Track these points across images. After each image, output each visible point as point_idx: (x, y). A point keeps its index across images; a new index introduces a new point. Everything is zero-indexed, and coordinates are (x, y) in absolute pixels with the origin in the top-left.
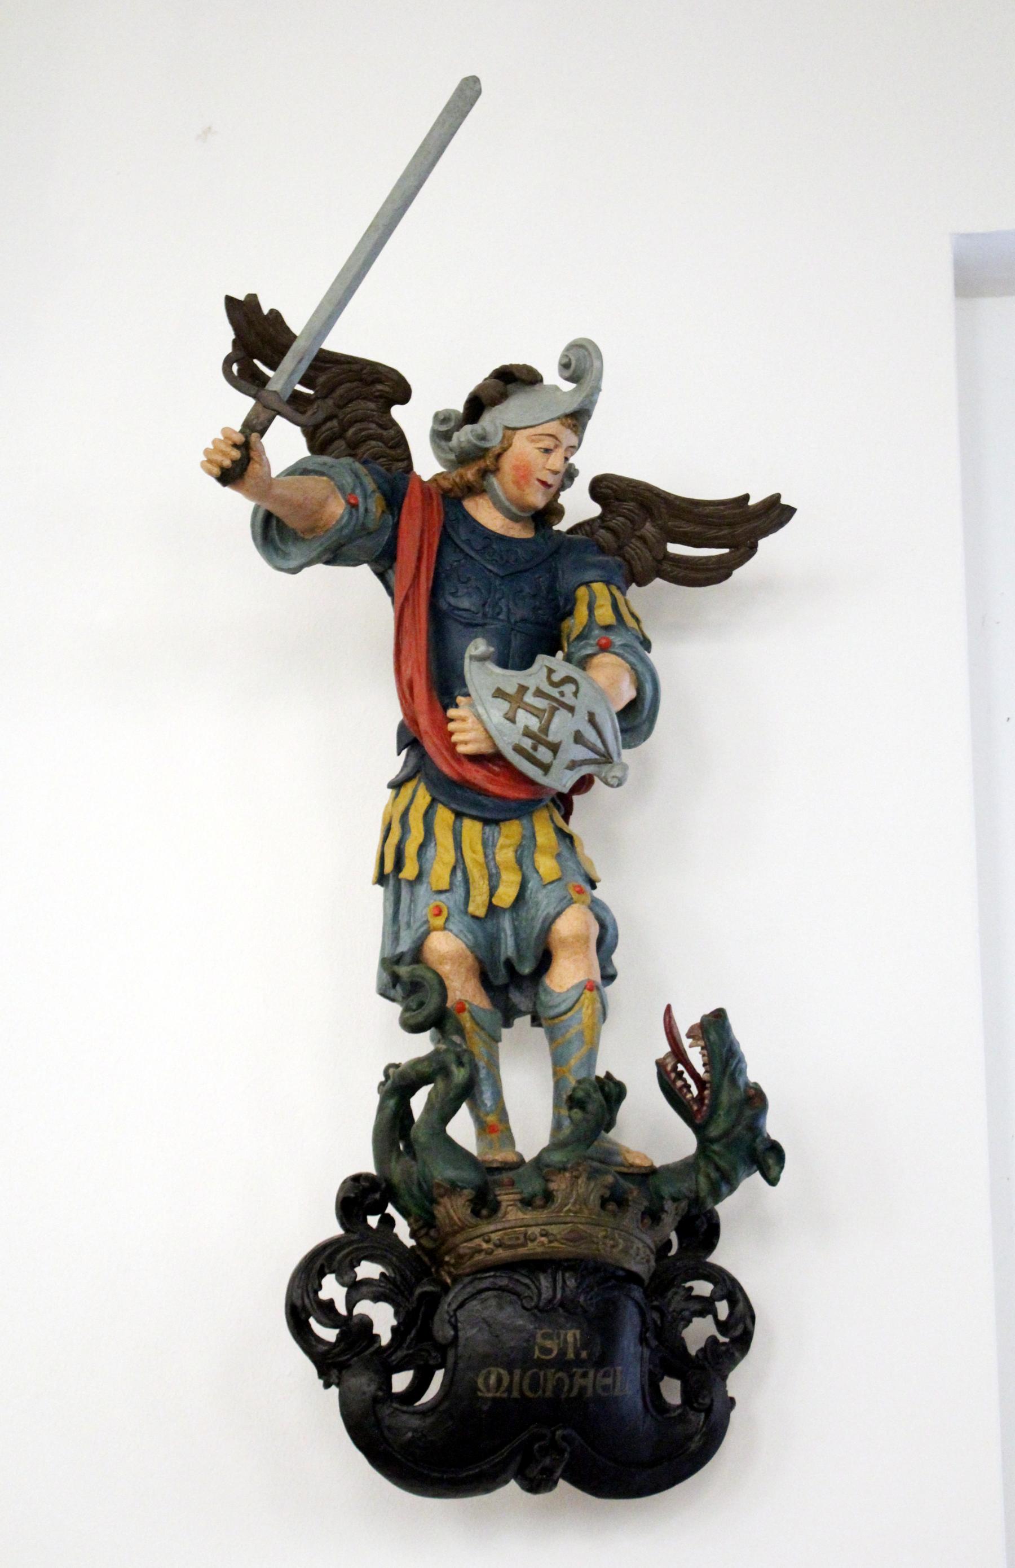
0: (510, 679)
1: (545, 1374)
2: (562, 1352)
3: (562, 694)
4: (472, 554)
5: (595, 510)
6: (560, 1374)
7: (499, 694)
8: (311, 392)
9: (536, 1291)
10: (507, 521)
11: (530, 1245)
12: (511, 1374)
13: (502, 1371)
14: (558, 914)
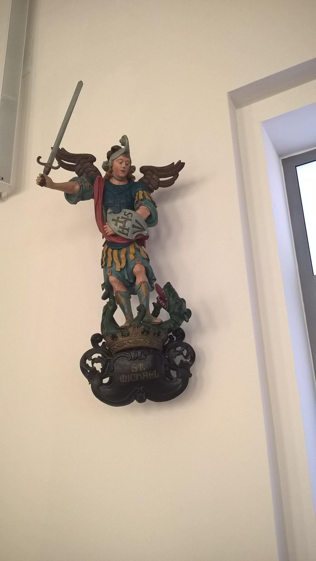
0: (115, 216)
1: (135, 375)
2: (139, 370)
3: (128, 217)
4: (111, 191)
5: (142, 175)
6: (139, 375)
7: (113, 220)
8: (75, 164)
9: (130, 356)
10: (119, 182)
11: (125, 345)
12: (127, 376)
13: (125, 376)
14: (134, 267)
